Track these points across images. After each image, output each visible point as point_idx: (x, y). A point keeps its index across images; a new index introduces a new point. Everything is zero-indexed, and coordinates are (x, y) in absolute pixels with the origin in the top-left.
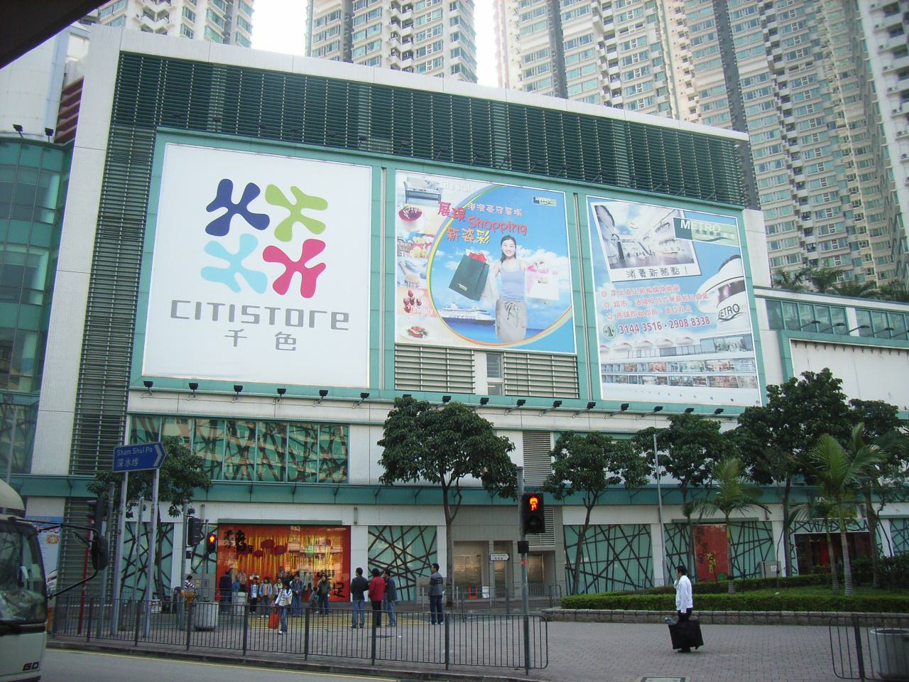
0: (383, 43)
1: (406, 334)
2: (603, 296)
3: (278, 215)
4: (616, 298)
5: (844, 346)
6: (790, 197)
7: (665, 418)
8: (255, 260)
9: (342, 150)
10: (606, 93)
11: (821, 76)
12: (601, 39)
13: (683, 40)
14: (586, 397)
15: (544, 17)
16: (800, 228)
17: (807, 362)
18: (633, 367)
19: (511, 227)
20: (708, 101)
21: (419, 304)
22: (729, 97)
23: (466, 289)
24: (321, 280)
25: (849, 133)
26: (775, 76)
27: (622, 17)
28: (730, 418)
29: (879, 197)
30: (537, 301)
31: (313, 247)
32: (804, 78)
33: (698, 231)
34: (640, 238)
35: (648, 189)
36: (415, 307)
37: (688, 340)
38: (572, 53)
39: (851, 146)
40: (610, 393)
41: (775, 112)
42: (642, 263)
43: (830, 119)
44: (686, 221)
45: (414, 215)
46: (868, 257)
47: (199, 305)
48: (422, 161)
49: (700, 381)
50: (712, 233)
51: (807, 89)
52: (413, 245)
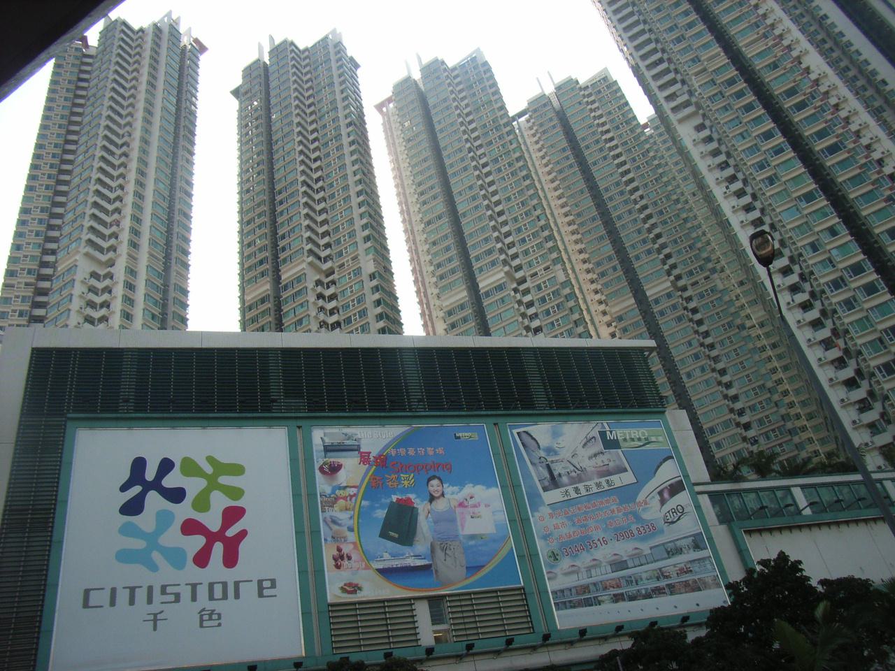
0: (311, 318)
1: (339, 593)
2: (540, 521)
3: (193, 486)
4: (554, 521)
5: (800, 527)
6: (721, 397)
7: (626, 638)
8: (173, 537)
9: (255, 415)
10: (527, 332)
11: (720, 287)
12: (515, 285)
13: (590, 276)
14: (542, 628)
15: (459, 274)
16: (738, 425)
17: (764, 549)
18: (585, 589)
19: (436, 466)
20: (624, 325)
21: (349, 558)
22: (643, 318)
23: (396, 536)
24: (244, 547)
25: (760, 332)
26: (680, 293)
27: (530, 264)
28: (699, 625)
29: (801, 384)
30: (472, 537)
31: (233, 515)
32: (706, 291)
33: (625, 440)
34: (568, 455)
35: (568, 408)
36: (346, 562)
37: (637, 551)
38: (490, 301)
39: (765, 342)
40: (565, 620)
41: (688, 324)
42: (574, 481)
43: (738, 321)
44: (611, 432)
45: (334, 469)
46: (810, 440)
47: (114, 591)
48: (378, 414)
49: (658, 591)
50: (639, 439)
51: (711, 299)
52: (337, 499)
